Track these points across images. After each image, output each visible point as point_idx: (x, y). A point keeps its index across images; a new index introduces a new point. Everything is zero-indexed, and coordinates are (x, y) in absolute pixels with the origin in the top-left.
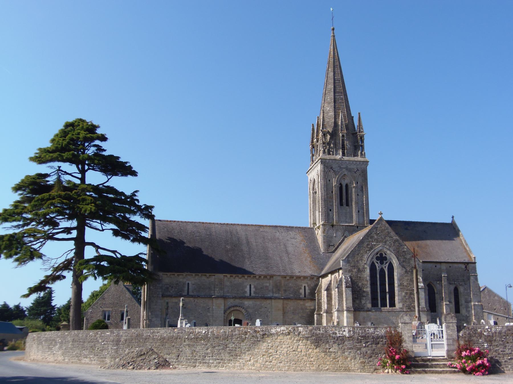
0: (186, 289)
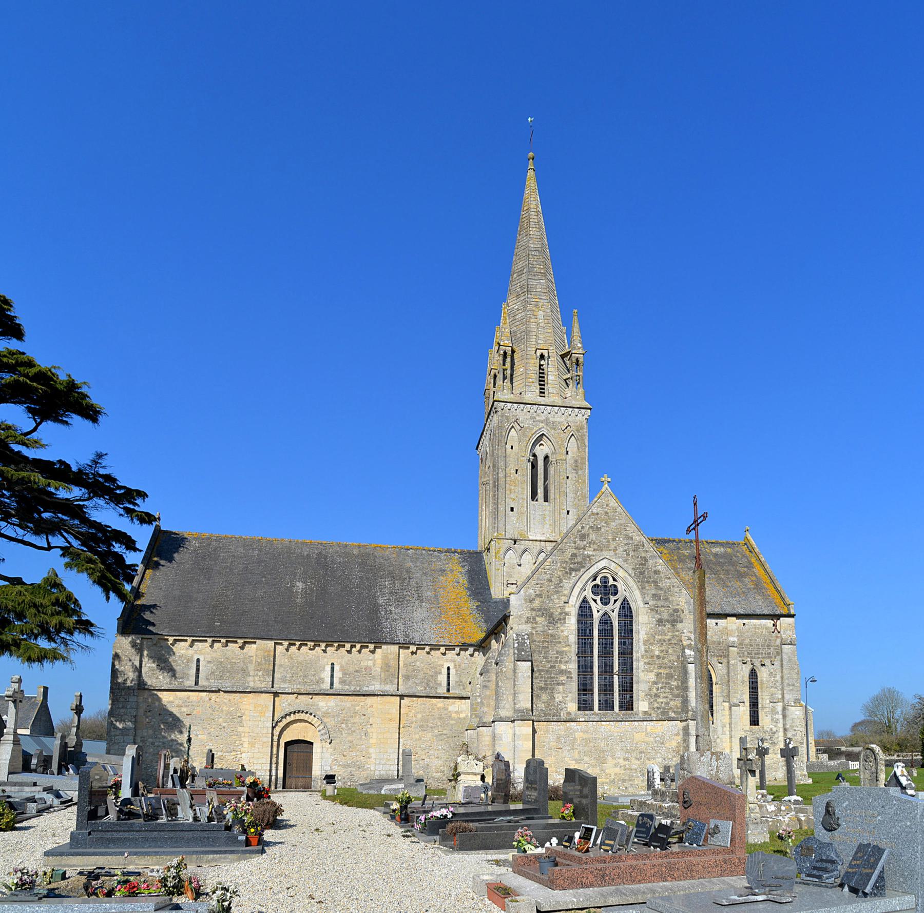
0: (193, 671)
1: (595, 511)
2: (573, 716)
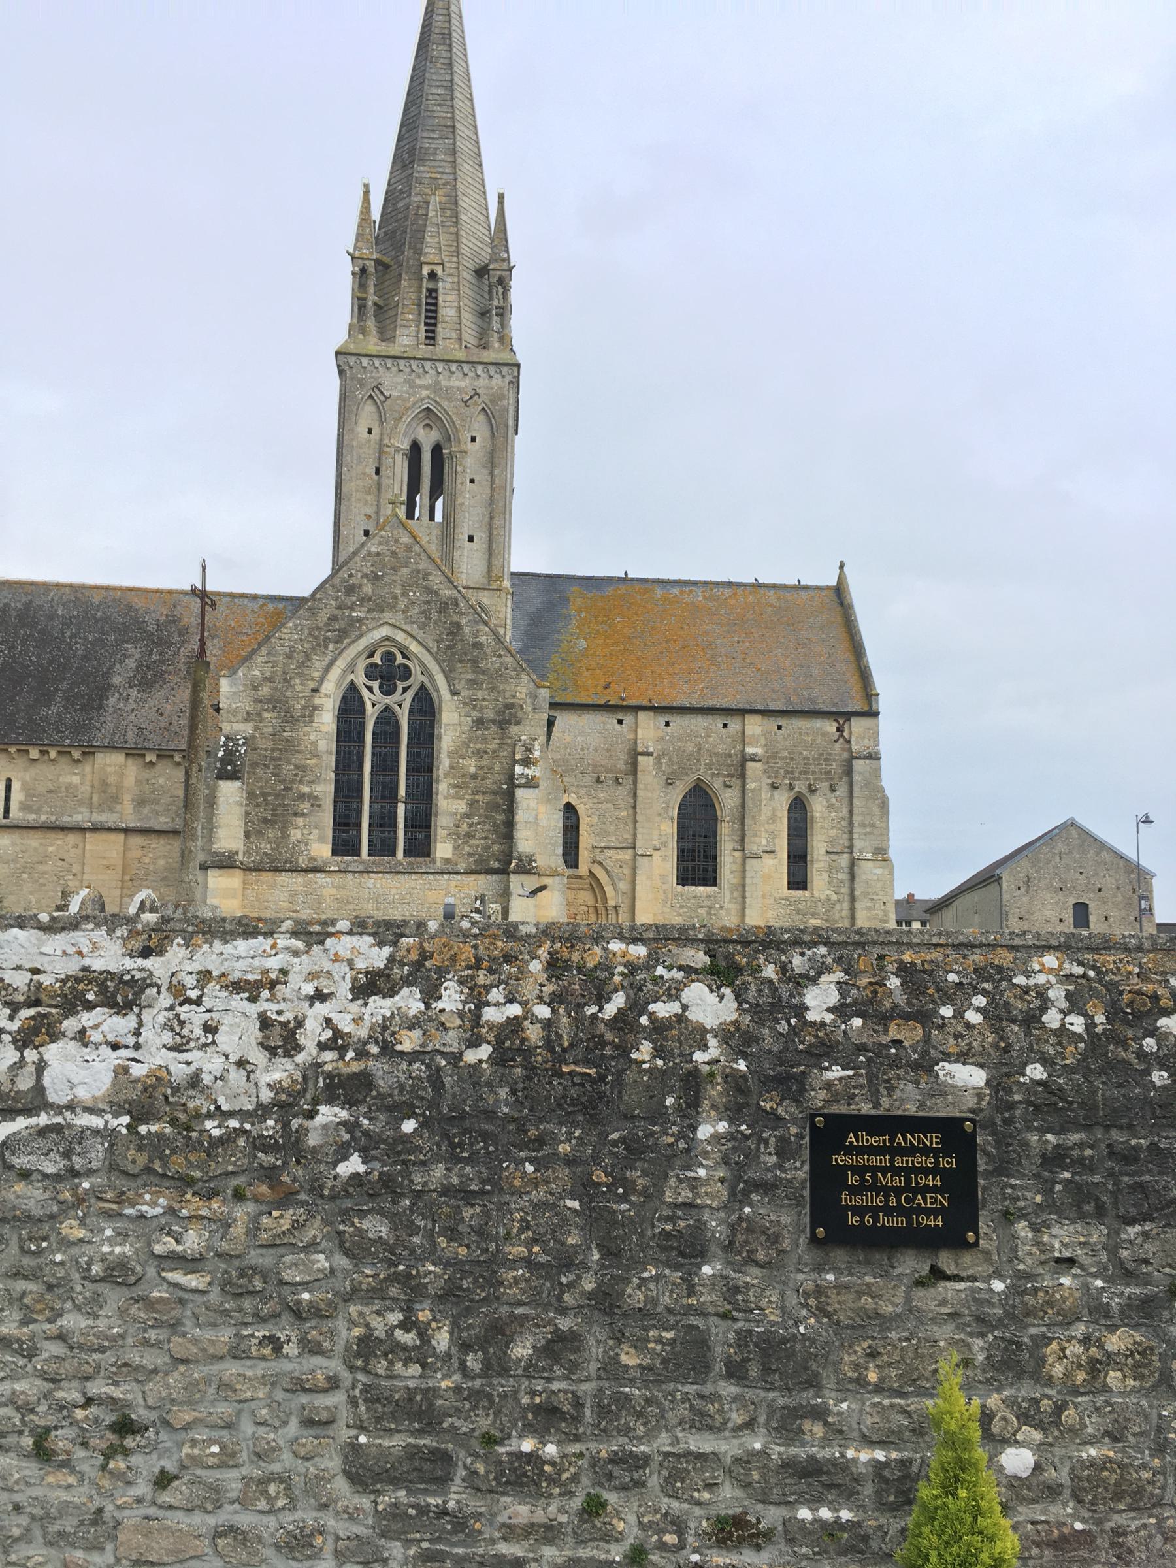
1: (374, 549)
2: (319, 863)
